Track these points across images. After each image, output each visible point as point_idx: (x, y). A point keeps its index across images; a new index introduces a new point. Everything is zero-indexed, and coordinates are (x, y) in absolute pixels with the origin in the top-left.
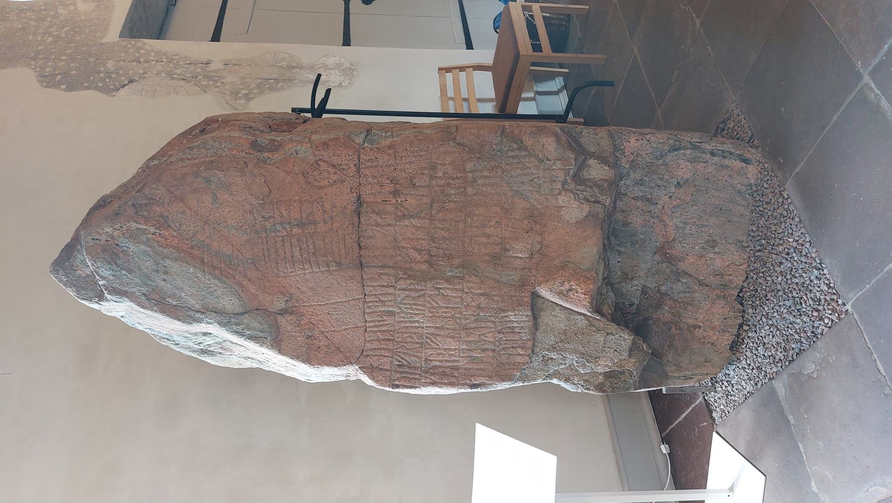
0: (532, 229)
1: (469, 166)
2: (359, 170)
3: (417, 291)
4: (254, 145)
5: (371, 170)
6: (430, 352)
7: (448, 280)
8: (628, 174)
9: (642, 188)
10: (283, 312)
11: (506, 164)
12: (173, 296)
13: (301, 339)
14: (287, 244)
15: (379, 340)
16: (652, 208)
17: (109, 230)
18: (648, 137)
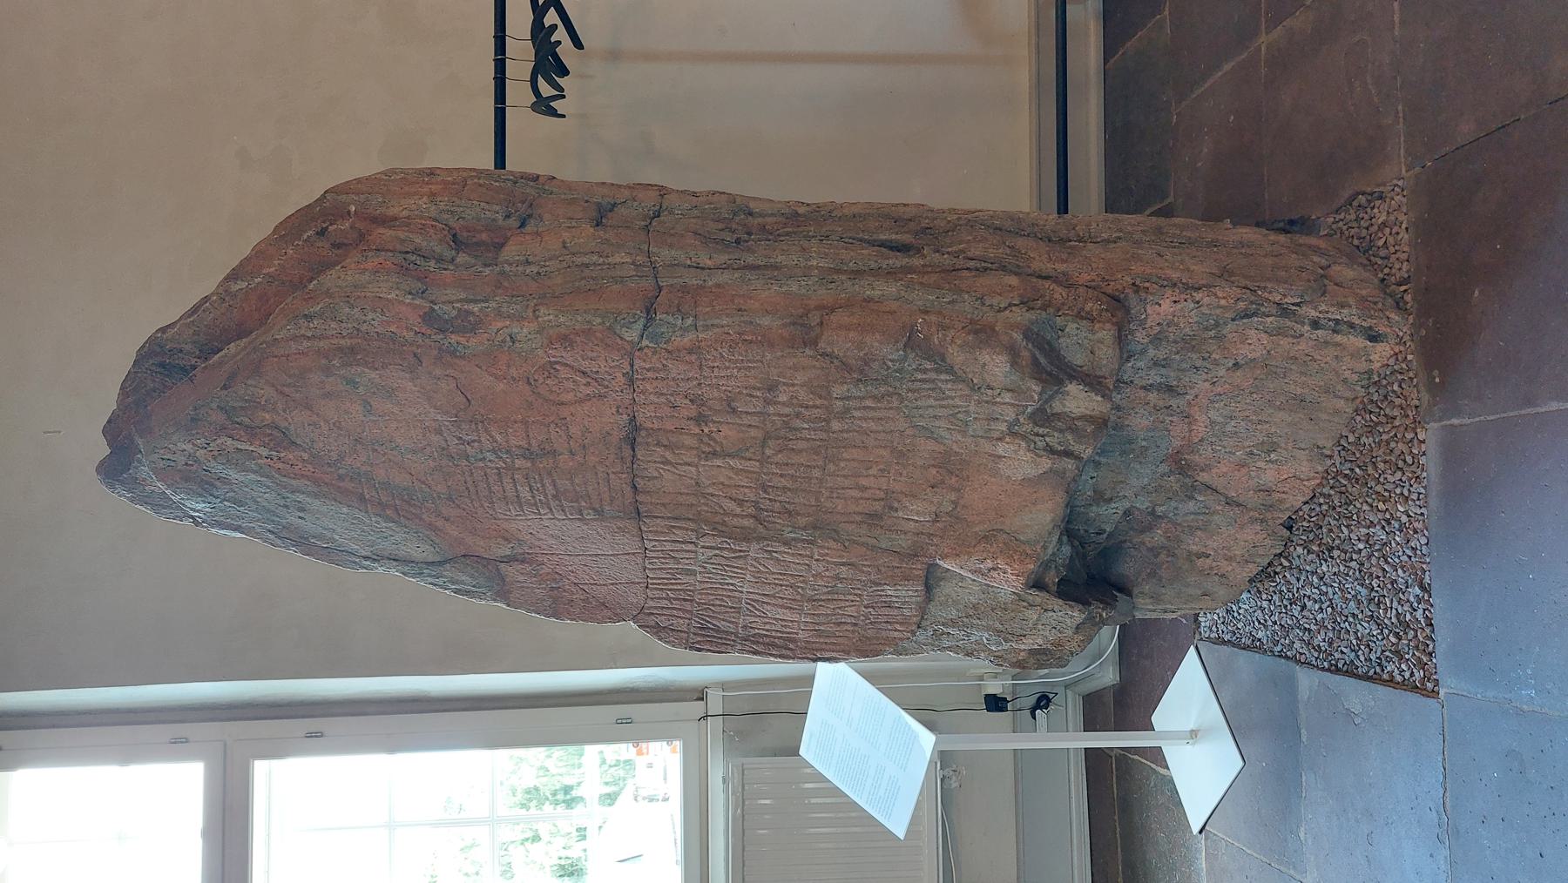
0: (943, 482)
1: (837, 391)
2: (631, 382)
3: (735, 551)
4: (429, 317)
5: (655, 383)
7: (786, 543)
8: (1143, 352)
9: (1163, 371)
10: (509, 560)
11: (909, 390)
12: (320, 537)
14: (507, 480)
15: (668, 599)
16: (1173, 402)
17: (188, 447)
18: (1198, 296)
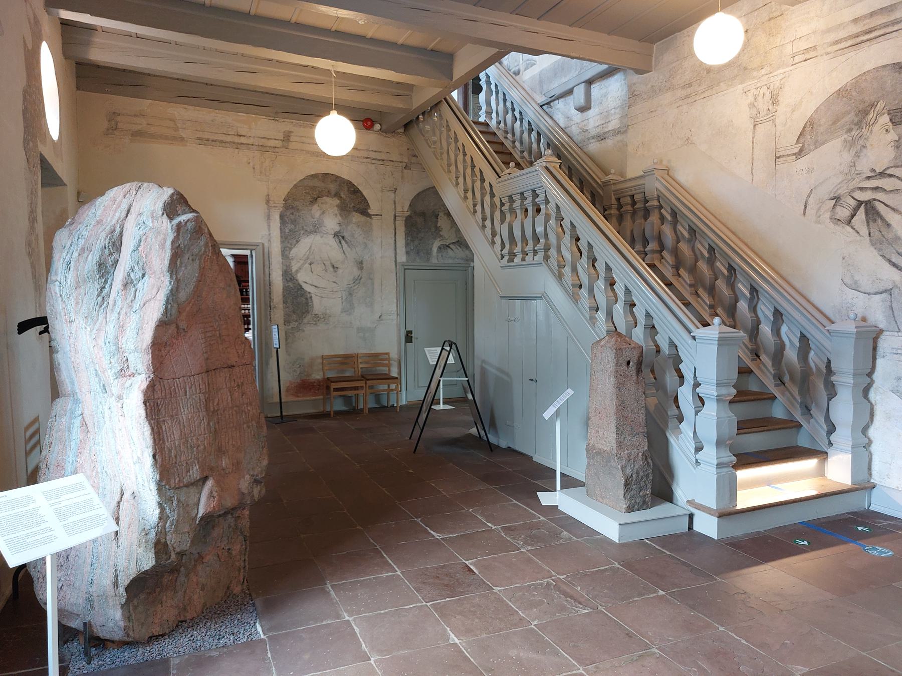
1: (254, 422)
6: (169, 422)
7: (209, 424)
10: (178, 327)
13: (165, 339)
15: (170, 388)
